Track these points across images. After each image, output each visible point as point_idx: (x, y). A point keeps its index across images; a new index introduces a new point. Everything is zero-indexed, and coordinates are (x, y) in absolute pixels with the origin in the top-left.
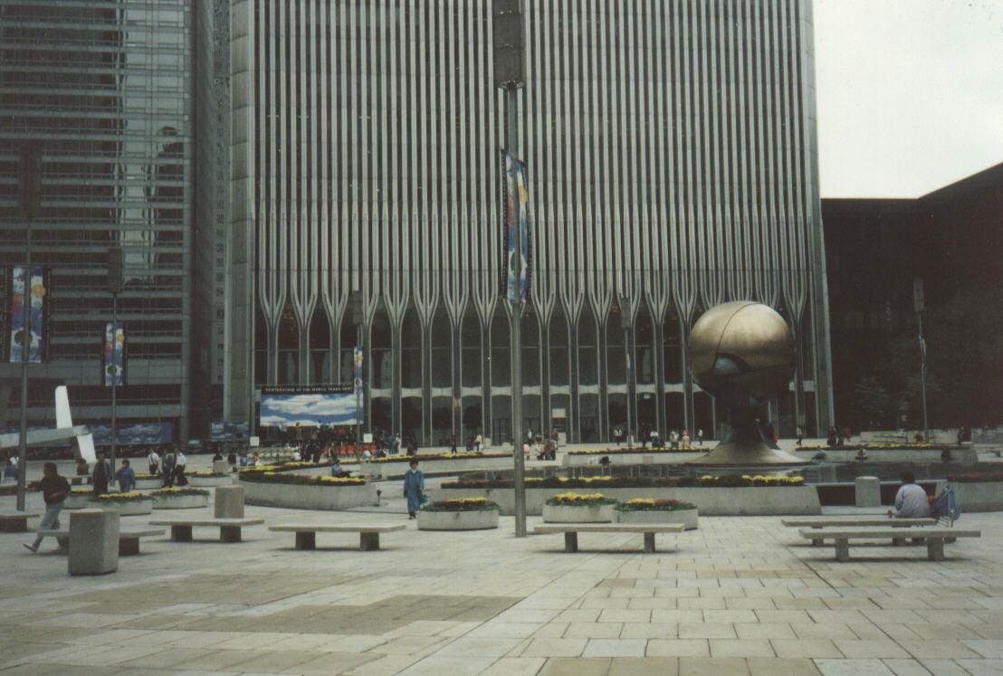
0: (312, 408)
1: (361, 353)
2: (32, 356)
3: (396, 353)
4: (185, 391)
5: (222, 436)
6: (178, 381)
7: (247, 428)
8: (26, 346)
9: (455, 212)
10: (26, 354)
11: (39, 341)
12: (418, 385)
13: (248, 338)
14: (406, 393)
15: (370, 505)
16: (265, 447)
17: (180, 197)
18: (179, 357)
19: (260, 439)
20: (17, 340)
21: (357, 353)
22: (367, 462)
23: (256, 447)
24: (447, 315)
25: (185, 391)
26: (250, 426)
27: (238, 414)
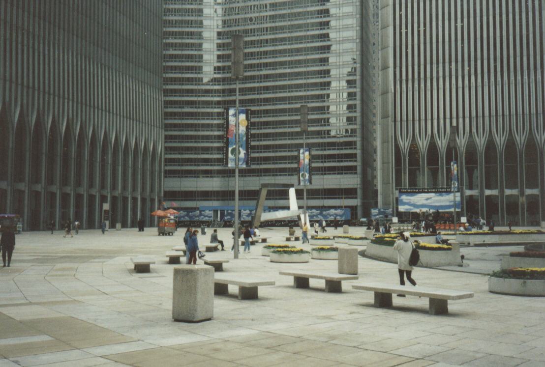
0: (429, 201)
1: (455, 166)
2: (240, 163)
3: (481, 169)
4: (359, 192)
5: (377, 217)
6: (355, 187)
7: (391, 212)
8: (237, 158)
9: (519, 78)
10: (237, 162)
11: (244, 153)
12: (496, 188)
13: (390, 161)
14: (488, 192)
15: (455, 265)
16: (401, 223)
17: (355, 85)
18: (356, 173)
19: (398, 218)
20: (232, 153)
21: (453, 165)
22: (460, 234)
23: (396, 223)
24: (514, 144)
25: (359, 192)
26: (393, 211)
27: (386, 204)
